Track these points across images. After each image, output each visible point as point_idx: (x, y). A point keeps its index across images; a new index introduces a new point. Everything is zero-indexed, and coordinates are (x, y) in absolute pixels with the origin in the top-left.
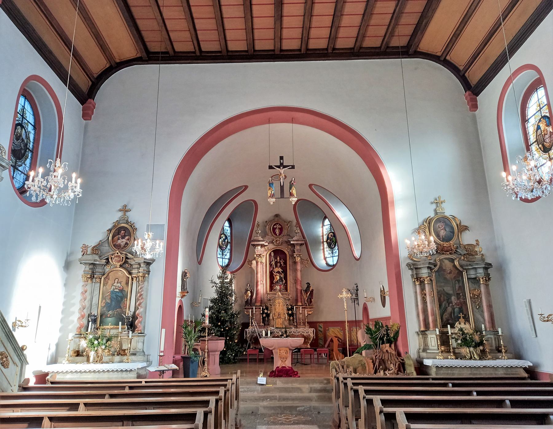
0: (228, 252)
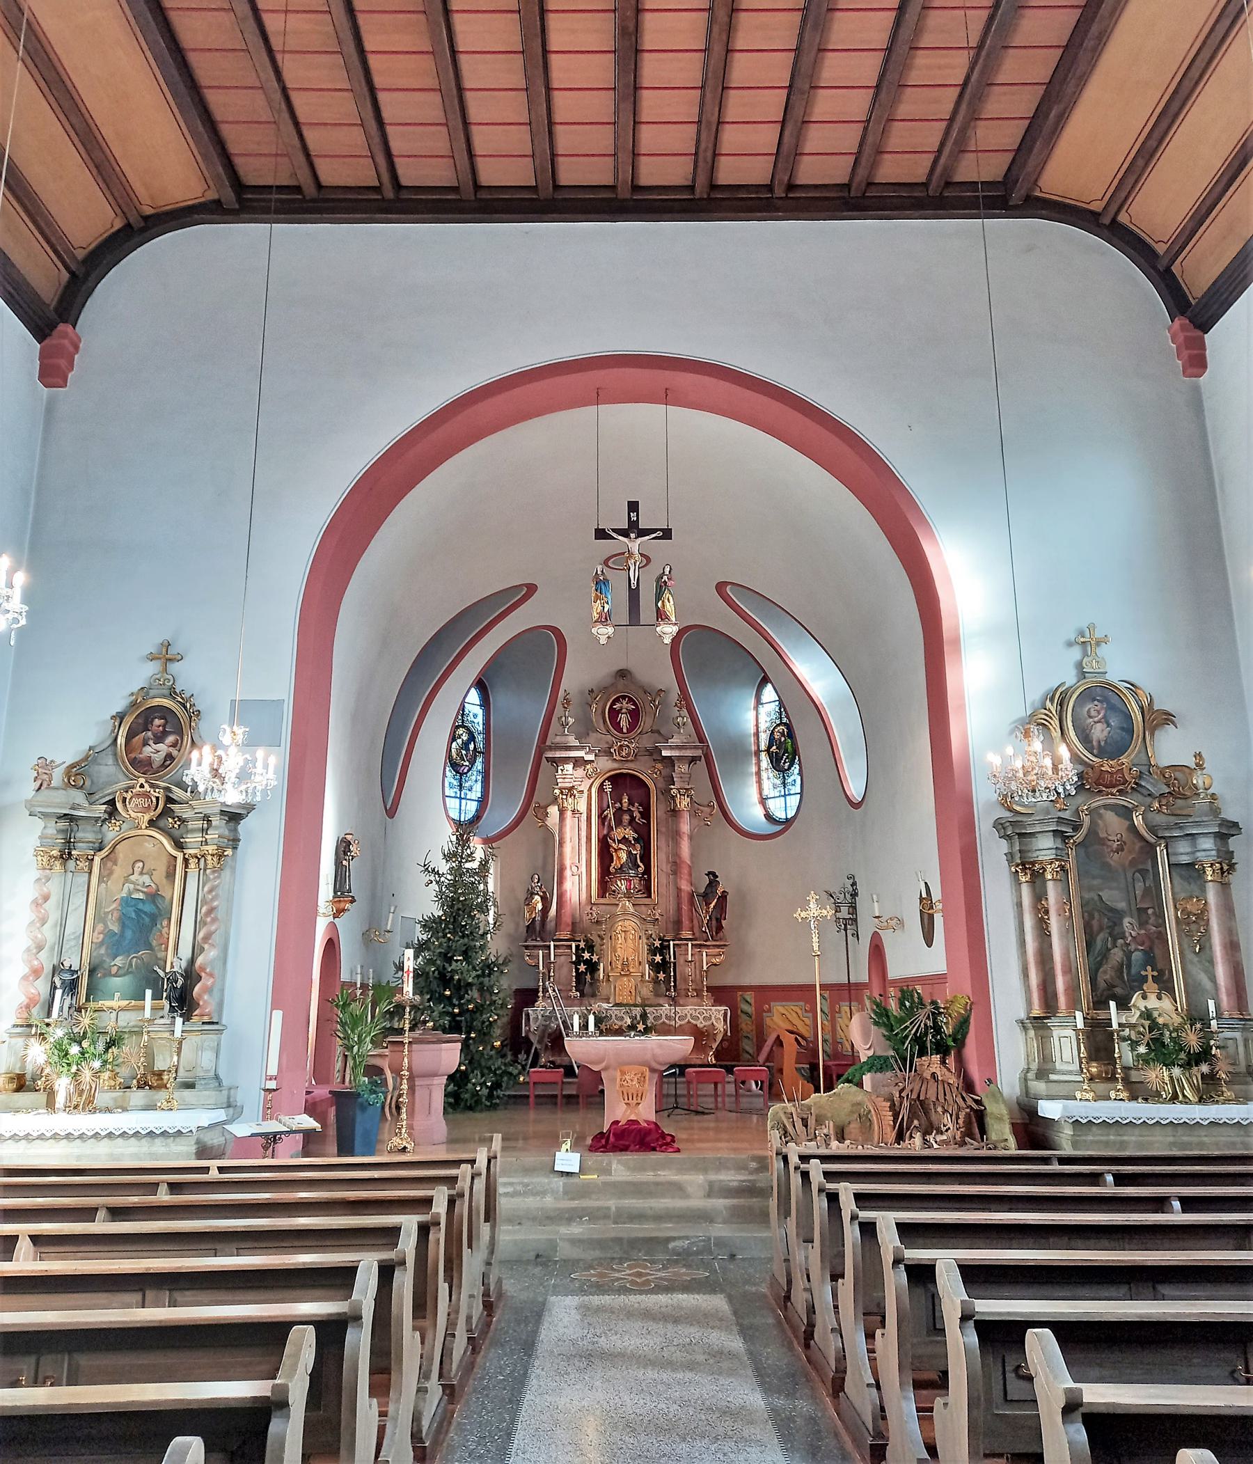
0: (476, 781)
